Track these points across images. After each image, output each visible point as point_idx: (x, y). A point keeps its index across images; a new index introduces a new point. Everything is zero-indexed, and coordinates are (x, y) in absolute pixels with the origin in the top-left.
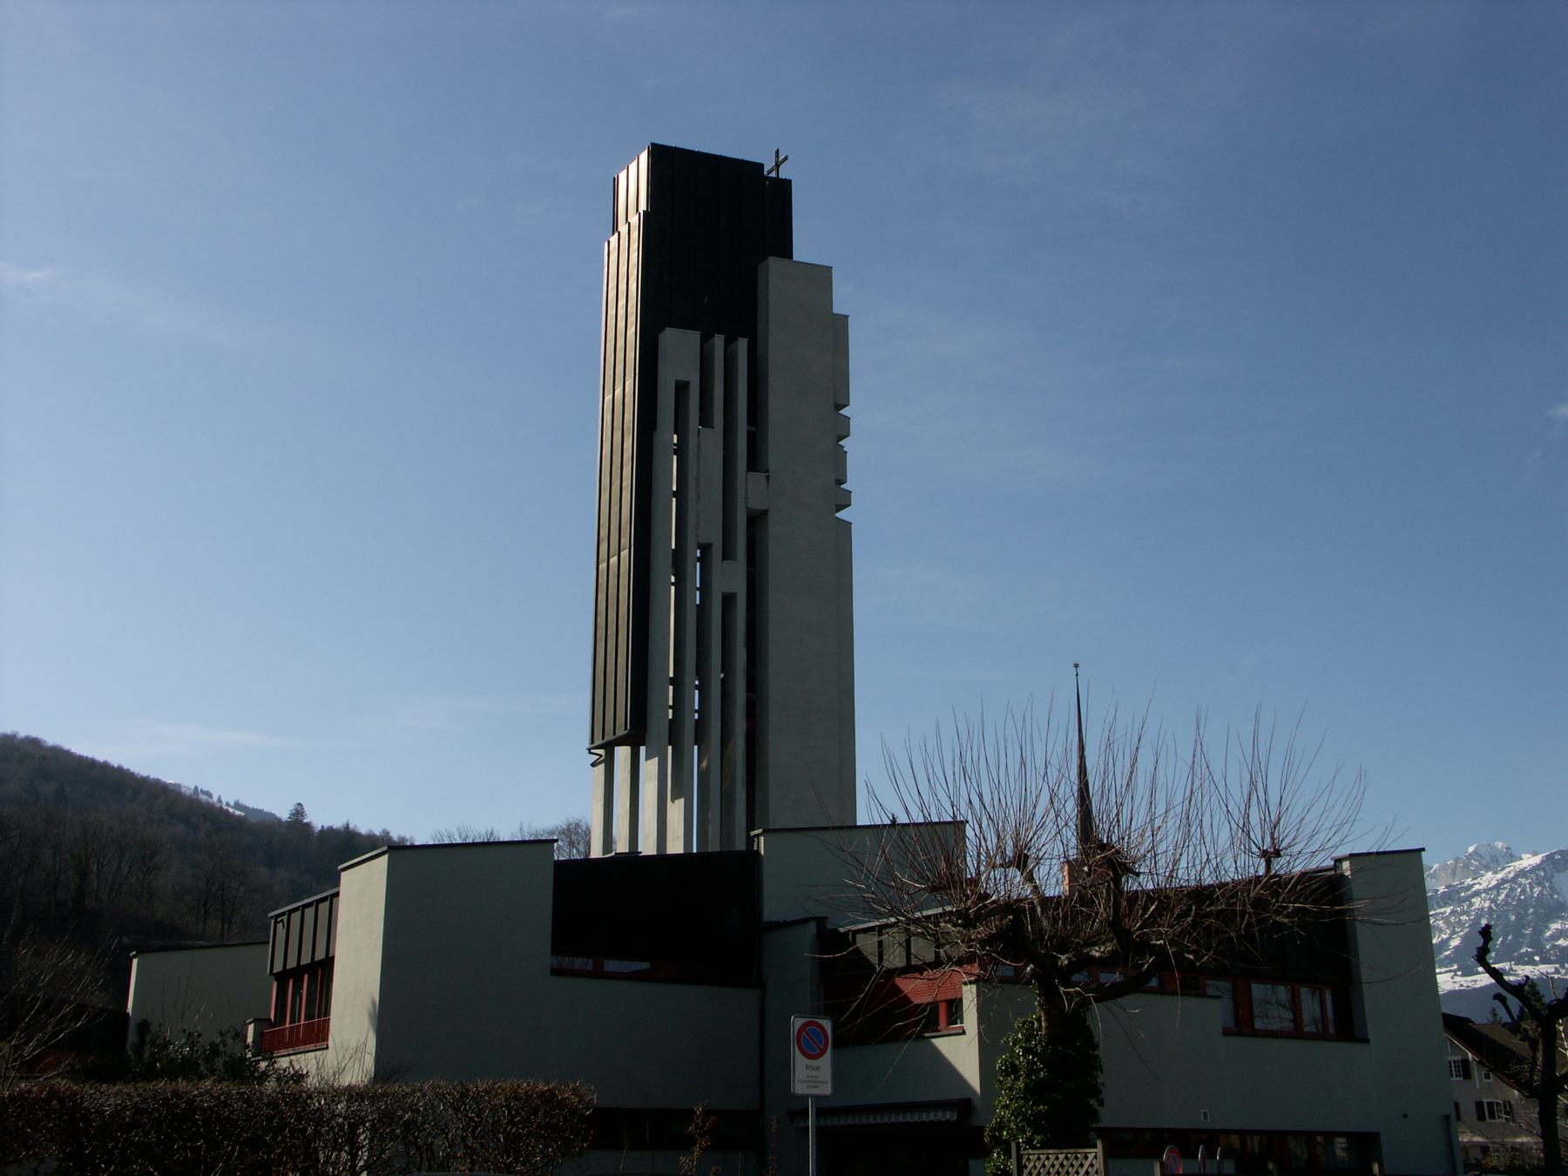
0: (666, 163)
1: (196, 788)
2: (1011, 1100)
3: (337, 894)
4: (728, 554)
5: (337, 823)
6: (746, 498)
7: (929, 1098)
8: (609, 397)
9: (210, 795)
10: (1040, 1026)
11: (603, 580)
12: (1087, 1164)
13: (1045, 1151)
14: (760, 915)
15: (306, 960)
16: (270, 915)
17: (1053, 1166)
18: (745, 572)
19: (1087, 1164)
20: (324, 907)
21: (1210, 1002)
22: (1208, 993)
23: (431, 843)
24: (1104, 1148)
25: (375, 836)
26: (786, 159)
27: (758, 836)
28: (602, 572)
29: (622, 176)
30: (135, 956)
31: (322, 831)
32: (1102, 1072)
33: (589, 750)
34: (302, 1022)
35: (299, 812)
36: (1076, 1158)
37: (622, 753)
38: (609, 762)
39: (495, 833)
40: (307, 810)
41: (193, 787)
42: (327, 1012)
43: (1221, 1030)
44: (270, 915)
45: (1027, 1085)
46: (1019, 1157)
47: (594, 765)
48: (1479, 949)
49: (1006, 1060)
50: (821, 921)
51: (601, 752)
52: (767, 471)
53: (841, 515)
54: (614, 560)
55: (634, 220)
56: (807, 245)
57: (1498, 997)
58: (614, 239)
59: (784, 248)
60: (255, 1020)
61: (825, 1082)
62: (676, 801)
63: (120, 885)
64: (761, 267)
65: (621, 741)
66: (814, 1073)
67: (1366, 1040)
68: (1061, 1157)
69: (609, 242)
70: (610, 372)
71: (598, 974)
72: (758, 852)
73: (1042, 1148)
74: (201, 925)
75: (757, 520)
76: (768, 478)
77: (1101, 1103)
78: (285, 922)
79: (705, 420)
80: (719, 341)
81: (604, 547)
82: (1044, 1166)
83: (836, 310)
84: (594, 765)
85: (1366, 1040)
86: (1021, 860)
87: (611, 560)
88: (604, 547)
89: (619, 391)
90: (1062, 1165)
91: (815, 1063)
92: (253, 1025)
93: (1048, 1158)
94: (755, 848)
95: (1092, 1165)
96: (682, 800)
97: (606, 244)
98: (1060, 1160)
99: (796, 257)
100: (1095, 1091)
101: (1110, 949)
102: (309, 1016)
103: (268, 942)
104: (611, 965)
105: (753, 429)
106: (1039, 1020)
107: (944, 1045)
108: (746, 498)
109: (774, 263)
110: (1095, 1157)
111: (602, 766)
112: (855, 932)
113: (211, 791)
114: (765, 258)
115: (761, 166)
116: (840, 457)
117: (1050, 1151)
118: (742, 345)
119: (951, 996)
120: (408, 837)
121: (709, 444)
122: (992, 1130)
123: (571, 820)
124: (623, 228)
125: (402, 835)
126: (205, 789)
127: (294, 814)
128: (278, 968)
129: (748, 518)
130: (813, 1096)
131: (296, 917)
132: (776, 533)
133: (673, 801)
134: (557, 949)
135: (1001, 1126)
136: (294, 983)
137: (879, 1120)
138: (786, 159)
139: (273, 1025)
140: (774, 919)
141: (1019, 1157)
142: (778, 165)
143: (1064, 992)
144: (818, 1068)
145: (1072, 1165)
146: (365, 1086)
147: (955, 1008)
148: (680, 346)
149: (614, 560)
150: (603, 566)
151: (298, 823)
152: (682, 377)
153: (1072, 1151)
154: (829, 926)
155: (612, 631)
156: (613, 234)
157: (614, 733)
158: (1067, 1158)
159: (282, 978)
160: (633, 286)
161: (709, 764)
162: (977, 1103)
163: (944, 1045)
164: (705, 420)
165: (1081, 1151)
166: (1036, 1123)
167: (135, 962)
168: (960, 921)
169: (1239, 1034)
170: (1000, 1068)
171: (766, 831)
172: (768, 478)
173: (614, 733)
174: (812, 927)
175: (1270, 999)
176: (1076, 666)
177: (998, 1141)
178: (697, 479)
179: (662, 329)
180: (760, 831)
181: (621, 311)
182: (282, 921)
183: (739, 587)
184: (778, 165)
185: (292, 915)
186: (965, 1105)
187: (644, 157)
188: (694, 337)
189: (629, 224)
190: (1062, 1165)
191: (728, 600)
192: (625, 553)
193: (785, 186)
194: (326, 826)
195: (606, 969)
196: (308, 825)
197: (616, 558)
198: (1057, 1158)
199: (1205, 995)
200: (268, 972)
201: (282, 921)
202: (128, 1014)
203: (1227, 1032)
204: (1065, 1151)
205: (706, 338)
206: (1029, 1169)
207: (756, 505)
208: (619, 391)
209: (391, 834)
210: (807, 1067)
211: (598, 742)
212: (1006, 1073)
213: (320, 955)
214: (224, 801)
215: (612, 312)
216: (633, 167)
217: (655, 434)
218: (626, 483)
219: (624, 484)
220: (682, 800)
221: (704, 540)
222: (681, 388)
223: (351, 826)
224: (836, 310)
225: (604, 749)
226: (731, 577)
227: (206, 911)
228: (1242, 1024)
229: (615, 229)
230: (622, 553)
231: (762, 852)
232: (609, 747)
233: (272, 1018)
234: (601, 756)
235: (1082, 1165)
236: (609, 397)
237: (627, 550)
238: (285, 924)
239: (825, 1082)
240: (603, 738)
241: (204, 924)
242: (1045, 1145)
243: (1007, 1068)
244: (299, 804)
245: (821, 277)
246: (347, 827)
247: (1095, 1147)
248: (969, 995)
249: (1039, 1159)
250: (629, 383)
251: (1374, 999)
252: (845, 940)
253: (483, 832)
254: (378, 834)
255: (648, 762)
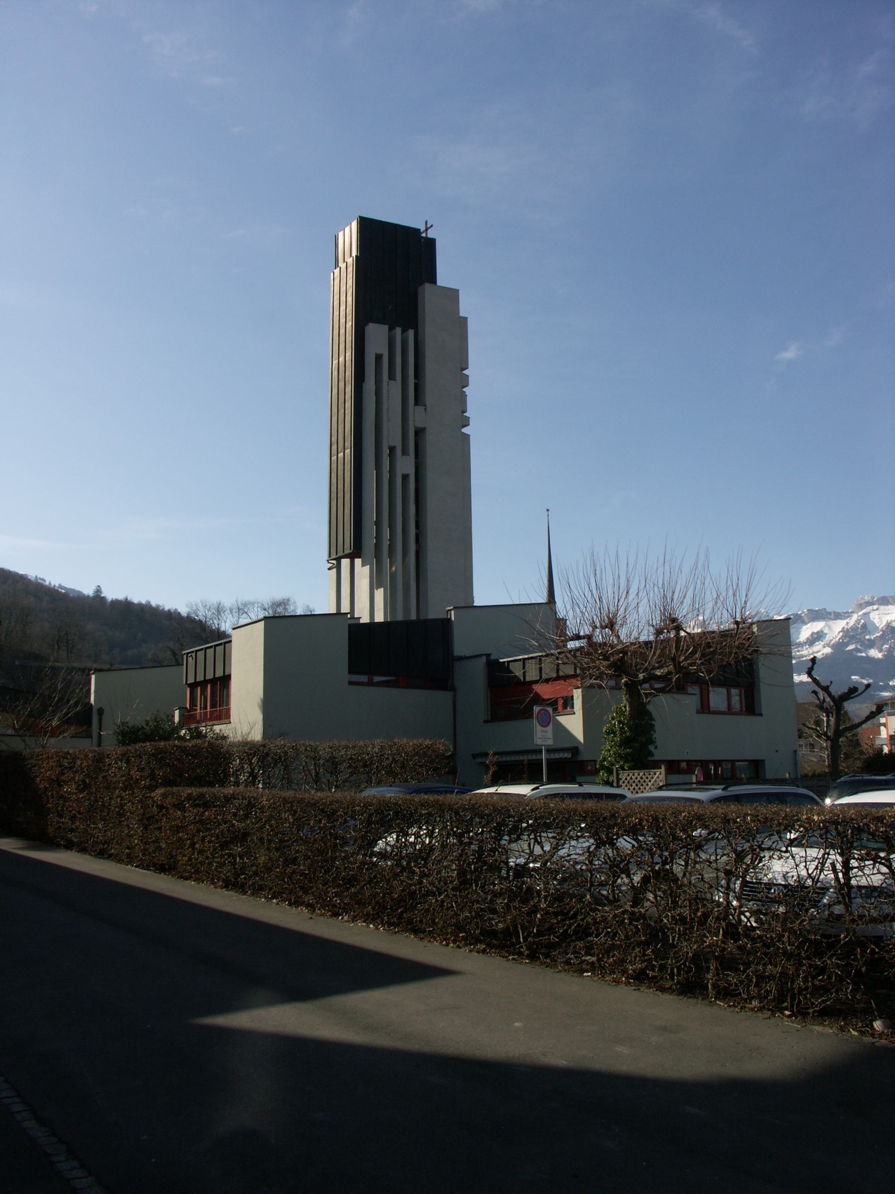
0: (368, 228)
1: (36, 577)
2: (611, 747)
3: (230, 641)
4: (405, 452)
5: (121, 597)
6: (414, 420)
7: (521, 749)
8: (335, 362)
9: (44, 581)
10: (626, 709)
11: (334, 466)
12: (653, 781)
13: (632, 771)
14: (452, 654)
15: (210, 676)
16: (183, 652)
17: (637, 778)
18: (414, 463)
19: (653, 781)
20: (220, 649)
21: (690, 696)
22: (689, 692)
23: (303, 614)
24: (665, 769)
25: (142, 604)
26: (432, 226)
27: (450, 610)
28: (334, 462)
29: (341, 234)
30: (93, 674)
31: (112, 601)
32: (655, 732)
33: (328, 561)
34: (209, 709)
35: (98, 591)
36: (650, 774)
37: (345, 563)
38: (338, 567)
39: (222, 603)
40: (103, 589)
41: (34, 576)
42: (228, 703)
43: (695, 711)
44: (183, 652)
45: (620, 740)
46: (618, 775)
47: (329, 569)
48: (809, 668)
49: (609, 727)
50: (488, 655)
51: (334, 562)
52: (425, 406)
53: (464, 430)
54: (341, 455)
55: (350, 261)
56: (445, 276)
57: (815, 692)
58: (337, 271)
59: (432, 278)
60: (179, 708)
61: (550, 739)
62: (379, 590)
63: (11, 631)
64: (420, 289)
65: (345, 557)
66: (546, 734)
67: (761, 715)
68: (641, 774)
69: (334, 273)
70: (335, 348)
71: (370, 683)
72: (450, 619)
73: (628, 770)
74: (56, 654)
75: (420, 433)
76: (425, 409)
77: (656, 748)
78: (194, 657)
79: (392, 377)
80: (398, 331)
81: (334, 447)
82: (631, 778)
83: (461, 315)
84: (329, 569)
85: (761, 715)
86: (611, 625)
87: (339, 455)
88: (334, 447)
89: (342, 359)
90: (642, 778)
91: (544, 729)
92: (178, 711)
93: (634, 775)
94: (449, 617)
95: (658, 777)
96: (382, 589)
97: (332, 274)
98: (641, 775)
99: (438, 284)
100: (652, 742)
101: (666, 671)
102: (213, 705)
103: (183, 665)
104: (376, 679)
105: (417, 381)
106: (625, 707)
107: (563, 720)
108: (414, 420)
109: (427, 286)
110: (660, 774)
111: (334, 570)
112: (509, 662)
113: (45, 578)
114: (422, 283)
115: (420, 230)
116: (464, 397)
117: (636, 771)
118: (411, 333)
119: (565, 694)
120: (161, 604)
121: (393, 391)
122: (601, 761)
123: (284, 597)
124: (342, 265)
125: (158, 603)
126: (42, 577)
127: (96, 592)
128: (191, 680)
129: (415, 432)
130: (544, 745)
131: (201, 655)
132: (430, 438)
133: (377, 589)
134: (351, 672)
135: (604, 759)
136: (211, 687)
137: (508, 759)
138: (432, 226)
139: (189, 711)
140: (460, 654)
141: (618, 775)
142: (427, 230)
143: (644, 693)
144: (546, 732)
145: (647, 778)
146: (232, 745)
147: (568, 702)
148: (377, 333)
149: (341, 455)
150: (334, 458)
151: (98, 597)
152: (379, 352)
153: (647, 771)
154: (493, 657)
155: (340, 495)
156: (336, 268)
157: (343, 552)
158: (644, 774)
159: (193, 686)
160: (350, 299)
161: (396, 569)
162: (581, 748)
163: (563, 720)
164: (392, 377)
165: (652, 770)
166: (625, 758)
167: (93, 677)
168: (600, 657)
169: (703, 713)
170: (606, 731)
171: (455, 608)
172: (425, 409)
173: (343, 552)
174: (484, 659)
175: (717, 698)
176: (548, 510)
177: (603, 767)
178: (388, 409)
179: (366, 324)
180: (452, 607)
181: (343, 313)
182: (191, 656)
183: (411, 470)
184: (427, 230)
185: (207, 650)
186: (575, 750)
187: (354, 225)
188: (386, 328)
189: (347, 263)
190: (642, 778)
191: (405, 477)
192: (348, 451)
193: (432, 242)
194: (114, 598)
195: (375, 681)
196: (104, 598)
197: (342, 454)
198: (639, 775)
199: (687, 693)
200: (184, 683)
201: (191, 656)
202: (92, 704)
203: (698, 712)
204: (644, 771)
205: (391, 329)
206: (623, 780)
207: (419, 425)
208: (342, 359)
209: (151, 603)
210: (542, 731)
211: (334, 556)
212: (608, 733)
213: (219, 673)
214: (53, 584)
215: (336, 313)
216: (347, 230)
217: (364, 385)
218: (348, 411)
219: (346, 412)
220: (382, 589)
221: (392, 444)
222: (379, 358)
223: (129, 599)
224: (461, 315)
225: (336, 561)
226: (406, 465)
227: (58, 646)
228: (704, 708)
229: (337, 265)
230: (346, 451)
231: (453, 619)
232: (338, 560)
233: (188, 706)
234: (334, 564)
235: (650, 781)
236: (335, 362)
237: (349, 450)
238: (194, 658)
239: (550, 739)
240: (337, 555)
241: (58, 654)
242: (630, 769)
243: (609, 731)
244: (99, 586)
245: (453, 295)
246: (126, 599)
247: (661, 768)
248: (578, 694)
249: (629, 775)
250: (348, 354)
251: (766, 695)
252: (505, 667)
253: (215, 602)
254: (144, 603)
255: (364, 568)
